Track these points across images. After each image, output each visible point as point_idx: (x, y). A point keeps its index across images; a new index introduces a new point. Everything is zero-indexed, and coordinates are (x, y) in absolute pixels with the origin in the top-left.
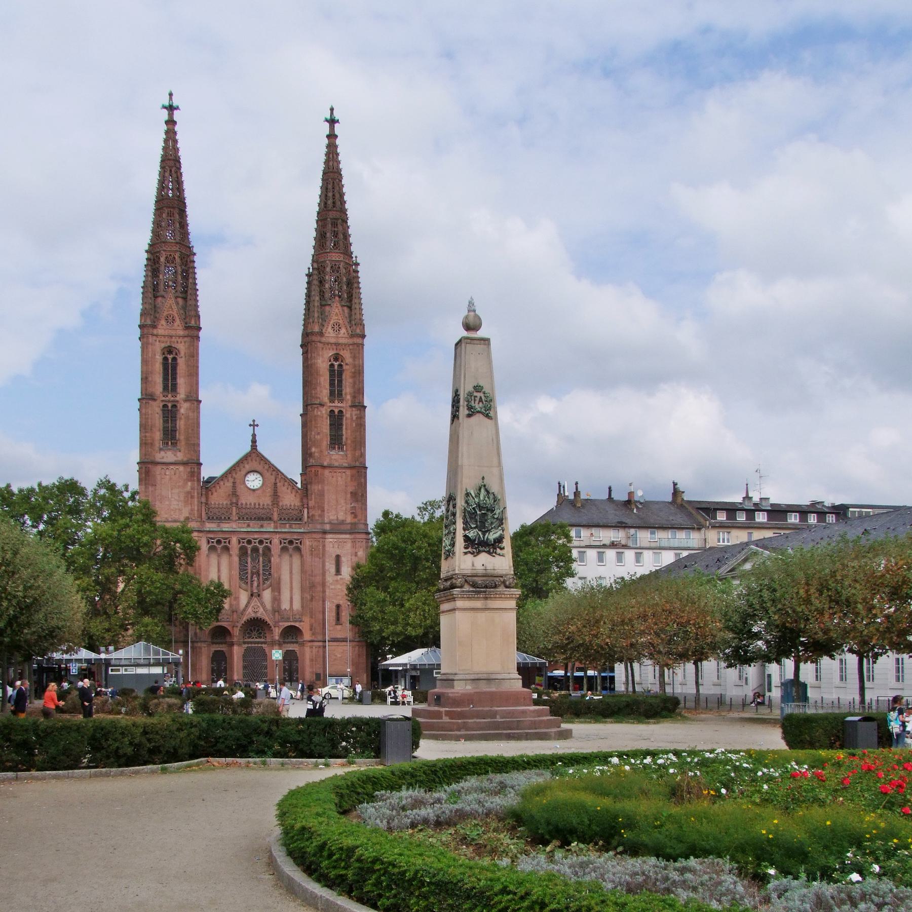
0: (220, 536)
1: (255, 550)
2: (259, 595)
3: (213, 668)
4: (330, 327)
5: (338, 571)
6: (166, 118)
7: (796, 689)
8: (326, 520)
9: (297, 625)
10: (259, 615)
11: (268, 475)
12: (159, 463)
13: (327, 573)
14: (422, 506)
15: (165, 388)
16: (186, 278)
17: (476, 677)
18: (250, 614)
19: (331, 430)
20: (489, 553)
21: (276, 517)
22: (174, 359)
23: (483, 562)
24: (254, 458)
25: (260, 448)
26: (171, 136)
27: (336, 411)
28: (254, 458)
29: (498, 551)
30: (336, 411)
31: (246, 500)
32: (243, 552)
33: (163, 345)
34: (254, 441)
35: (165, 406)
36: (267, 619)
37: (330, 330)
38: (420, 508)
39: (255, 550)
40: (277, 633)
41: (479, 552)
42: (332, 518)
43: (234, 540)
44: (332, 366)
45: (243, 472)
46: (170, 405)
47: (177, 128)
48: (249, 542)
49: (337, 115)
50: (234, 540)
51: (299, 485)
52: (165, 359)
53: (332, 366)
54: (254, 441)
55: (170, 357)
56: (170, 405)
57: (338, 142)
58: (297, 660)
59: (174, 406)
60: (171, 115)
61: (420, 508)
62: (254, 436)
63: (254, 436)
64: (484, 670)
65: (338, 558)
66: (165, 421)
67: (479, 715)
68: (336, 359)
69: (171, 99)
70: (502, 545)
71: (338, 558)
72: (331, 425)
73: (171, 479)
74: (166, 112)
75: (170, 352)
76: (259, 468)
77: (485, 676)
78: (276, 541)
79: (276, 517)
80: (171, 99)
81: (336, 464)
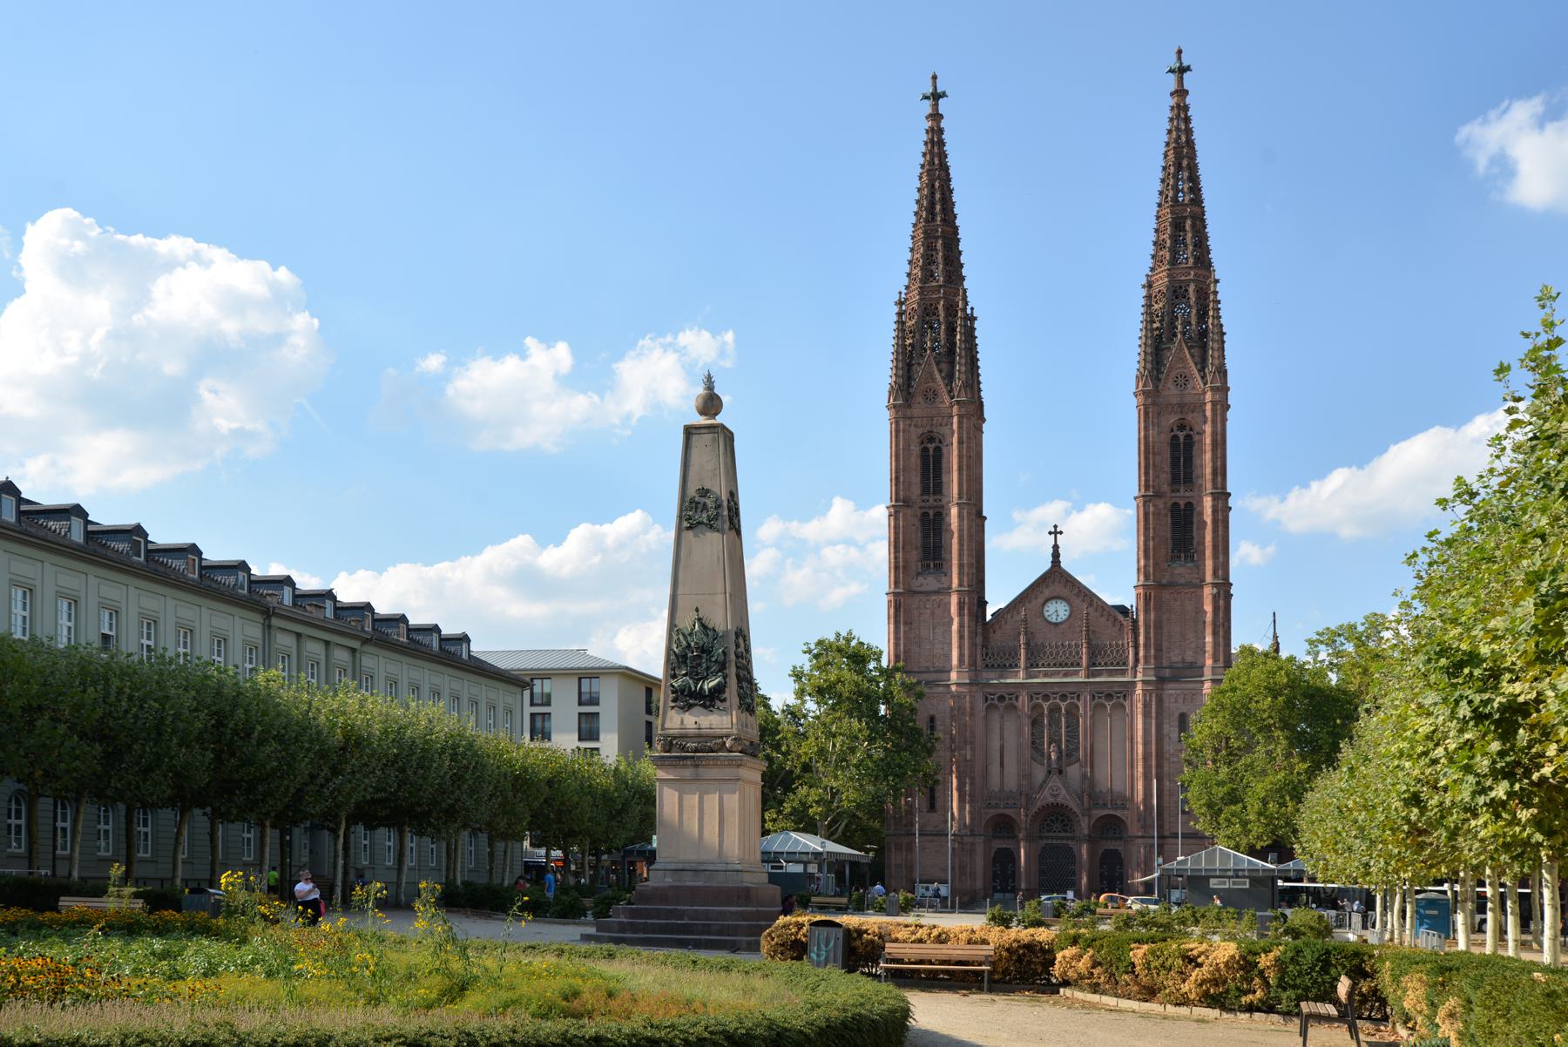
2: (1060, 772)
3: (994, 873)
4: (1170, 384)
6: (929, 111)
7: (410, 869)
8: (1165, 664)
9: (1118, 813)
10: (1059, 800)
11: (1077, 602)
12: (915, 592)
13: (1166, 739)
14: (1315, 637)
16: (1202, 316)
17: (681, 866)
18: (1045, 798)
19: (1173, 531)
20: (704, 706)
22: (938, 449)
24: (1056, 580)
25: (1065, 564)
26: (1181, 113)
27: (1182, 503)
28: (1056, 580)
29: (718, 703)
30: (1182, 503)
33: (920, 431)
35: (925, 514)
36: (1072, 805)
37: (1170, 384)
38: (1311, 642)
39: (1055, 709)
40: (1084, 826)
41: (690, 707)
42: (1175, 659)
44: (1175, 438)
45: (1041, 601)
46: (931, 513)
47: (943, 124)
52: (925, 450)
53: (1175, 438)
55: (931, 447)
56: (931, 513)
58: (1122, 865)
60: (936, 106)
61: (1311, 642)
62: (1056, 547)
63: (1056, 547)
64: (694, 857)
66: (925, 536)
67: (658, 914)
68: (1182, 427)
69: (1179, 58)
70: (726, 695)
72: (1173, 524)
73: (933, 613)
74: (1173, 78)
75: (931, 440)
77: (694, 866)
80: (1179, 58)
81: (1182, 581)
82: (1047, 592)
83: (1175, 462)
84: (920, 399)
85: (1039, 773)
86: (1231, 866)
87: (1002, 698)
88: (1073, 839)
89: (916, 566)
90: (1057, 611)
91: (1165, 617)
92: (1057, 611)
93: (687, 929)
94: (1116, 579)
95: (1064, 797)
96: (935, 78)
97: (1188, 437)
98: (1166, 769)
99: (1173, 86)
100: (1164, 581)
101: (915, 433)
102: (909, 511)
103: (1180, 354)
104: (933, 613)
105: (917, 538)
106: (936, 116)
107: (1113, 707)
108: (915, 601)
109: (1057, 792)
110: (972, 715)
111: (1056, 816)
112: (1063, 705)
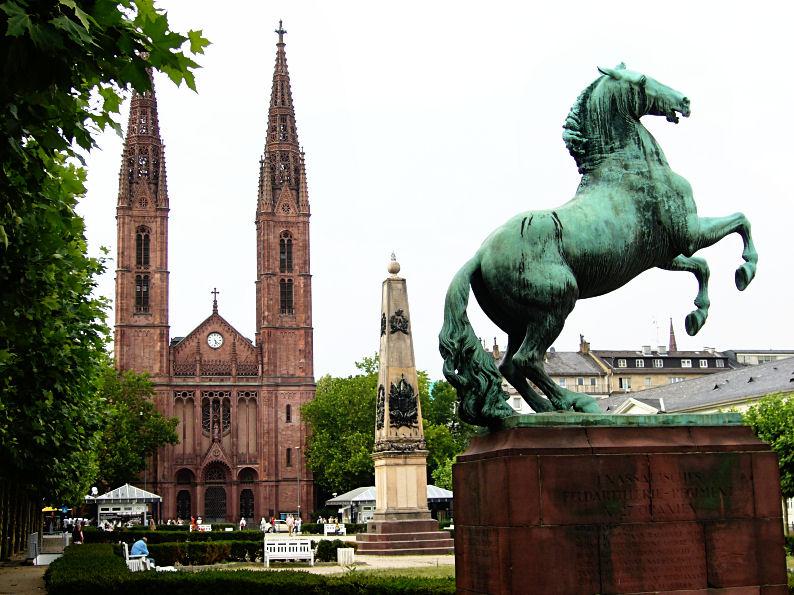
0: (185, 390)
1: (216, 401)
5: (289, 419)
8: (278, 375)
11: (227, 335)
15: (139, 262)
16: (157, 165)
18: (211, 457)
19: (282, 295)
21: (234, 372)
22: (147, 237)
23: (404, 432)
24: (215, 322)
26: (281, 58)
28: (215, 322)
31: (208, 357)
32: (205, 404)
34: (215, 306)
37: (280, 210)
43: (198, 393)
45: (206, 334)
46: (286, 280)
48: (211, 394)
49: (284, 28)
50: (198, 393)
51: (254, 344)
53: (282, 241)
54: (215, 306)
55: (143, 235)
56: (286, 280)
57: (286, 49)
59: (146, 277)
60: (281, 38)
62: (215, 302)
63: (215, 302)
65: (288, 407)
71: (288, 407)
73: (143, 340)
75: (143, 230)
76: (220, 330)
78: (234, 393)
79: (234, 372)
81: (287, 326)
82: (210, 329)
83: (139, 245)
84: (137, 205)
85: (206, 443)
86: (120, 497)
87: (185, 395)
88: (224, 483)
89: (133, 310)
90: (215, 341)
91: (278, 347)
92: (215, 341)
93: (414, 545)
94: (244, 321)
95: (221, 457)
96: (281, 22)
97: (289, 241)
98: (279, 439)
99: (277, 41)
100: (277, 326)
101: (134, 226)
102: (129, 274)
103: (285, 194)
104: (143, 340)
105: (133, 290)
106: (281, 45)
107: (249, 401)
108: (130, 332)
109: (218, 454)
110: (168, 405)
111: (217, 469)
112: (221, 399)
